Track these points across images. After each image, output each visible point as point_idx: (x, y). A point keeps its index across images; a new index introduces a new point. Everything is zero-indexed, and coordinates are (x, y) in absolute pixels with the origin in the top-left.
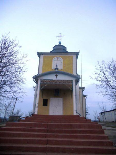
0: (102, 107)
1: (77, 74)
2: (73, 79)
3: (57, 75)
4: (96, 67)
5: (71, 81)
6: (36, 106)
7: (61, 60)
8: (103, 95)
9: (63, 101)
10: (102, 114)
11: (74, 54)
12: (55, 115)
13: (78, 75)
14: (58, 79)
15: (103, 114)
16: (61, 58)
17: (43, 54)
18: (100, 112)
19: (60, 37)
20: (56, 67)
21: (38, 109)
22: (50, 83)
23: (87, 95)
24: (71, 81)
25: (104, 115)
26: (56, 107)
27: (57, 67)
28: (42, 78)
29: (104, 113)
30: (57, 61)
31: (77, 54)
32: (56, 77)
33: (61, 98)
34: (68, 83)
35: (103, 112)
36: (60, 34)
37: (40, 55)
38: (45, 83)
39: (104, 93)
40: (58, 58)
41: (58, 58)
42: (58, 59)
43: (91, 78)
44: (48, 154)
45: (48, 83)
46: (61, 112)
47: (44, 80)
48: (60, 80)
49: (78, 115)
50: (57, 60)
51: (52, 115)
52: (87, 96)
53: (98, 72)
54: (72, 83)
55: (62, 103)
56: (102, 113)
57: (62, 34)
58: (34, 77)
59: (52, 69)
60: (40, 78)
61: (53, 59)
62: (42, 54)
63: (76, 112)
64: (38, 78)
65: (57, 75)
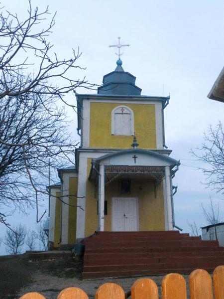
0: (209, 211)
1: (164, 146)
2: (165, 165)
3: (135, 157)
4: (205, 134)
5: (162, 169)
6: (101, 218)
7: (130, 114)
8: (217, 190)
9: (139, 202)
10: (207, 231)
11: (157, 101)
12: (128, 231)
13: (168, 149)
14: (137, 164)
15: (213, 230)
16: (130, 109)
17: (88, 99)
18: (203, 227)
19: (119, 47)
20: (134, 141)
21: (105, 221)
22: (123, 173)
23: (176, 186)
24: (162, 169)
25: (213, 233)
26: (124, 215)
27: (136, 141)
28: (108, 162)
29: (214, 228)
30: (121, 115)
31: (164, 101)
32: (135, 160)
33: (135, 197)
34: (157, 171)
35: (210, 224)
36: (119, 38)
37: (83, 99)
38: (115, 172)
39: (218, 185)
40: (123, 110)
41: (123, 110)
42: (124, 112)
43: (192, 154)
44: (146, 286)
45: (120, 173)
46: (136, 224)
47: (113, 166)
48: (142, 166)
49: (175, 229)
50: (122, 114)
51: (117, 230)
52: (176, 188)
53: (209, 145)
54: (164, 171)
55: (135, 210)
56: (208, 228)
57: (124, 41)
58: (94, 162)
59: (113, 133)
60: (103, 162)
61: (112, 110)
62: (87, 97)
63: (174, 226)
64: (100, 162)
65: (135, 157)
